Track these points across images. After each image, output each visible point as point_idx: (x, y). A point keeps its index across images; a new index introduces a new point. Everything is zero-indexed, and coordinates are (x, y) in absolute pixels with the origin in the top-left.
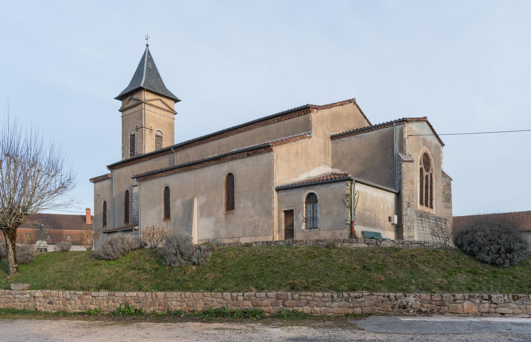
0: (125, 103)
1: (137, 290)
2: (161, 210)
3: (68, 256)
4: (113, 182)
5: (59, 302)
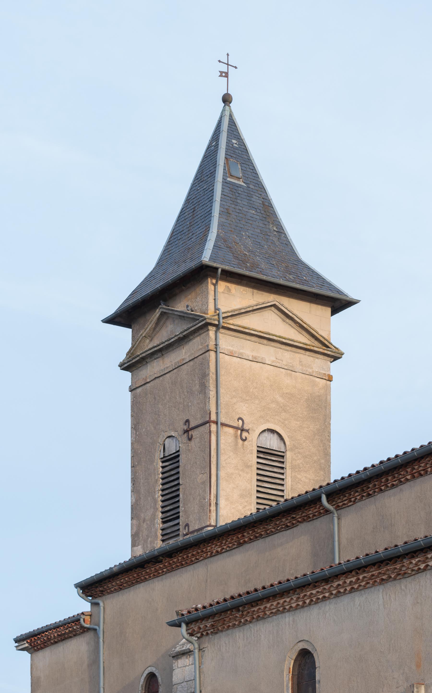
0: (143, 333)
4: (98, 643)
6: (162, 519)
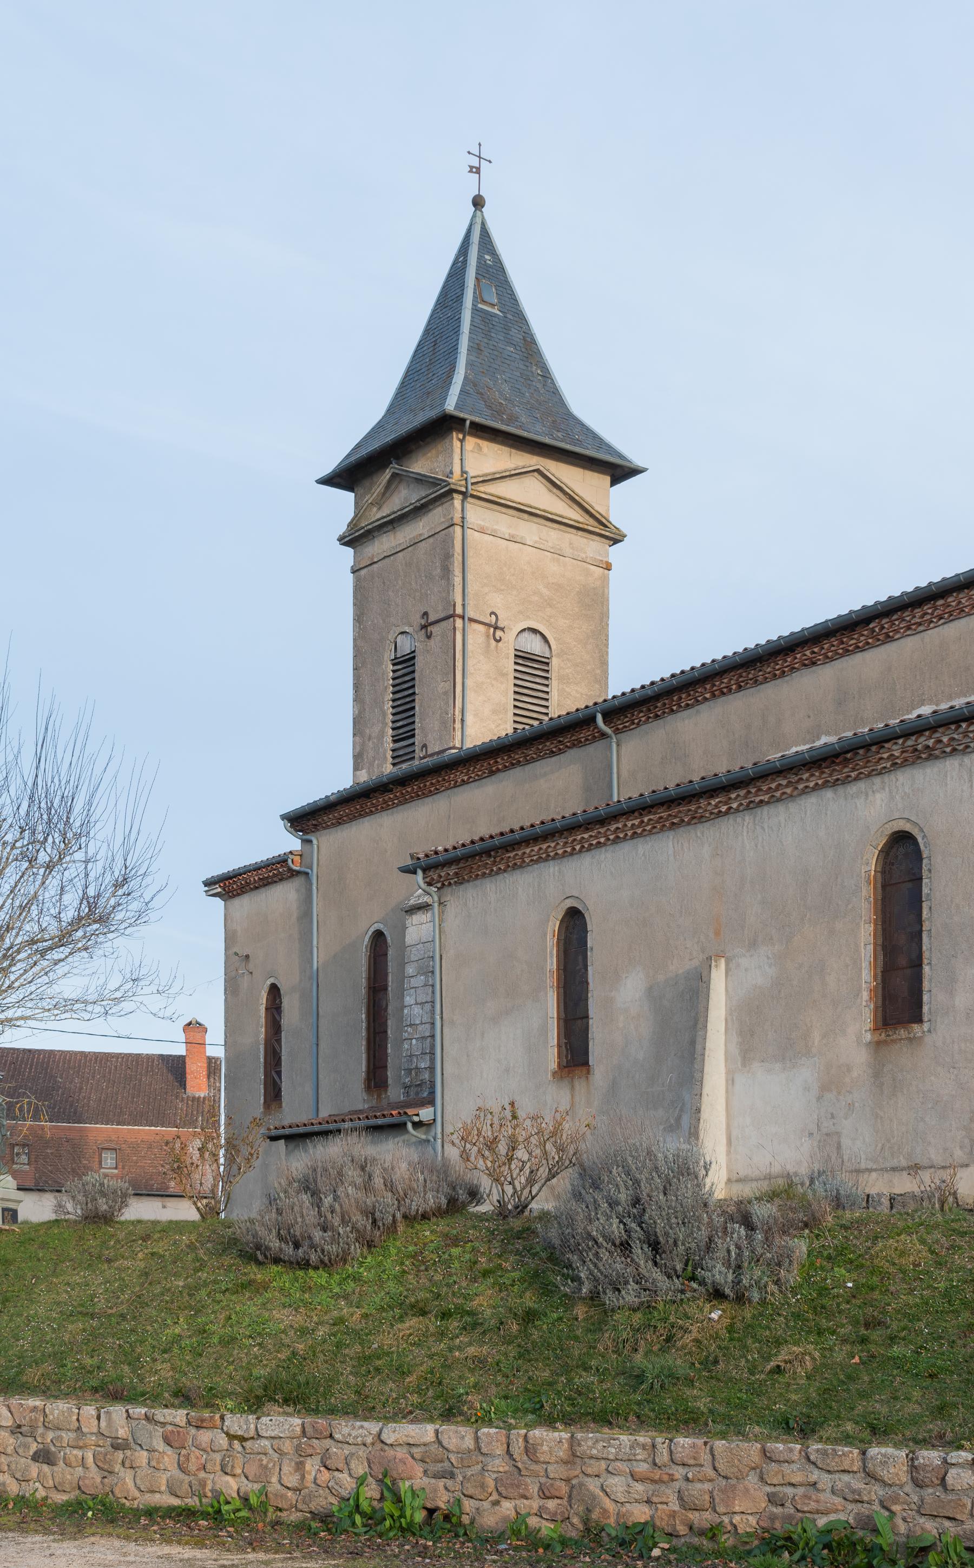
0: (369, 498)
1: (436, 1413)
2: (544, 1030)
3: (118, 1241)
4: (310, 890)
5: (79, 1453)
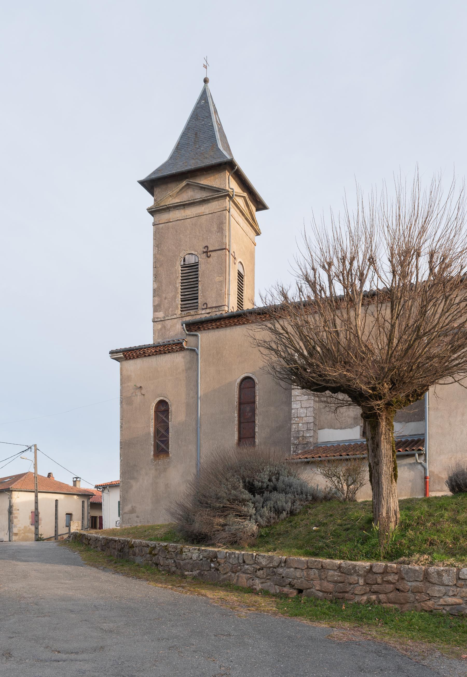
6: (181, 299)
